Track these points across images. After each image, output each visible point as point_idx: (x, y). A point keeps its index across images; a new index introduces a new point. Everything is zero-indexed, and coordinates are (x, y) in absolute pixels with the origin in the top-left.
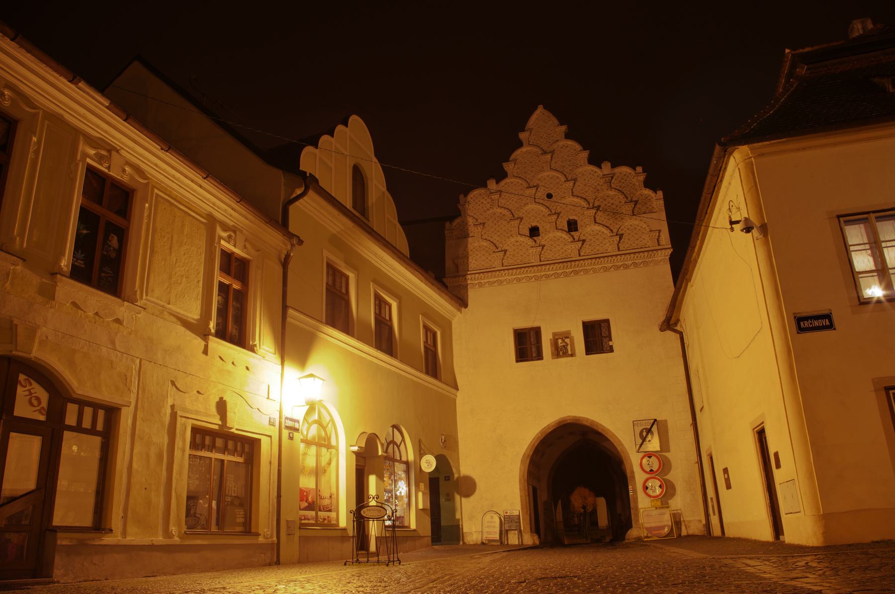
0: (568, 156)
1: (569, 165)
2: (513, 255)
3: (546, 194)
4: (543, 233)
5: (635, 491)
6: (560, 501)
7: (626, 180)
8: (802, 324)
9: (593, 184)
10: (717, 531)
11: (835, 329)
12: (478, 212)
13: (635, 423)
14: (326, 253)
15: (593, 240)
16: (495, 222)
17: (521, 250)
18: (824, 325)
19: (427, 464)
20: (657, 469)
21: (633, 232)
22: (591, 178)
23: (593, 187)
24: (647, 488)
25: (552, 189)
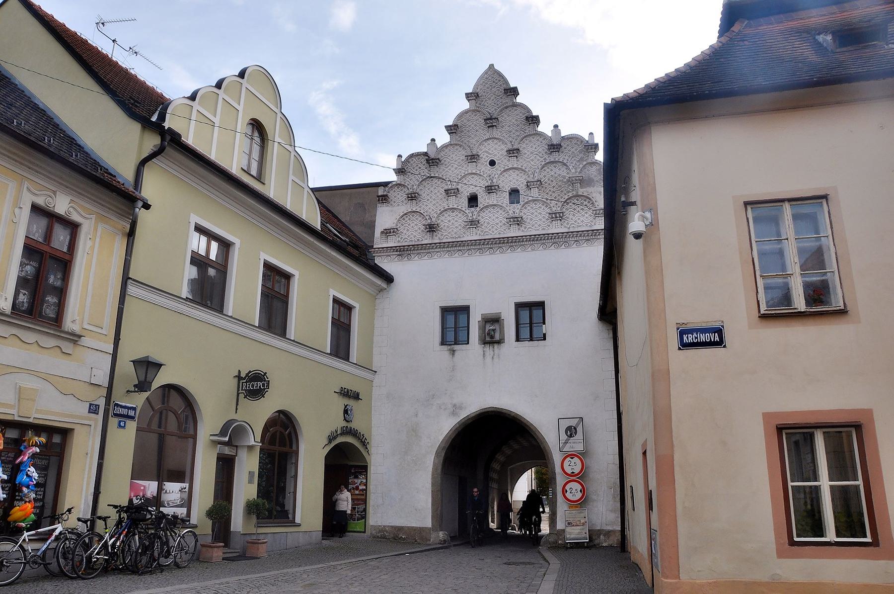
0: (516, 120)
2: (448, 227)
3: (489, 161)
8: (685, 338)
9: (540, 152)
11: (725, 346)
15: (535, 213)
17: (456, 221)
18: (713, 340)
21: (578, 207)
22: (539, 146)
23: (541, 155)
25: (495, 155)
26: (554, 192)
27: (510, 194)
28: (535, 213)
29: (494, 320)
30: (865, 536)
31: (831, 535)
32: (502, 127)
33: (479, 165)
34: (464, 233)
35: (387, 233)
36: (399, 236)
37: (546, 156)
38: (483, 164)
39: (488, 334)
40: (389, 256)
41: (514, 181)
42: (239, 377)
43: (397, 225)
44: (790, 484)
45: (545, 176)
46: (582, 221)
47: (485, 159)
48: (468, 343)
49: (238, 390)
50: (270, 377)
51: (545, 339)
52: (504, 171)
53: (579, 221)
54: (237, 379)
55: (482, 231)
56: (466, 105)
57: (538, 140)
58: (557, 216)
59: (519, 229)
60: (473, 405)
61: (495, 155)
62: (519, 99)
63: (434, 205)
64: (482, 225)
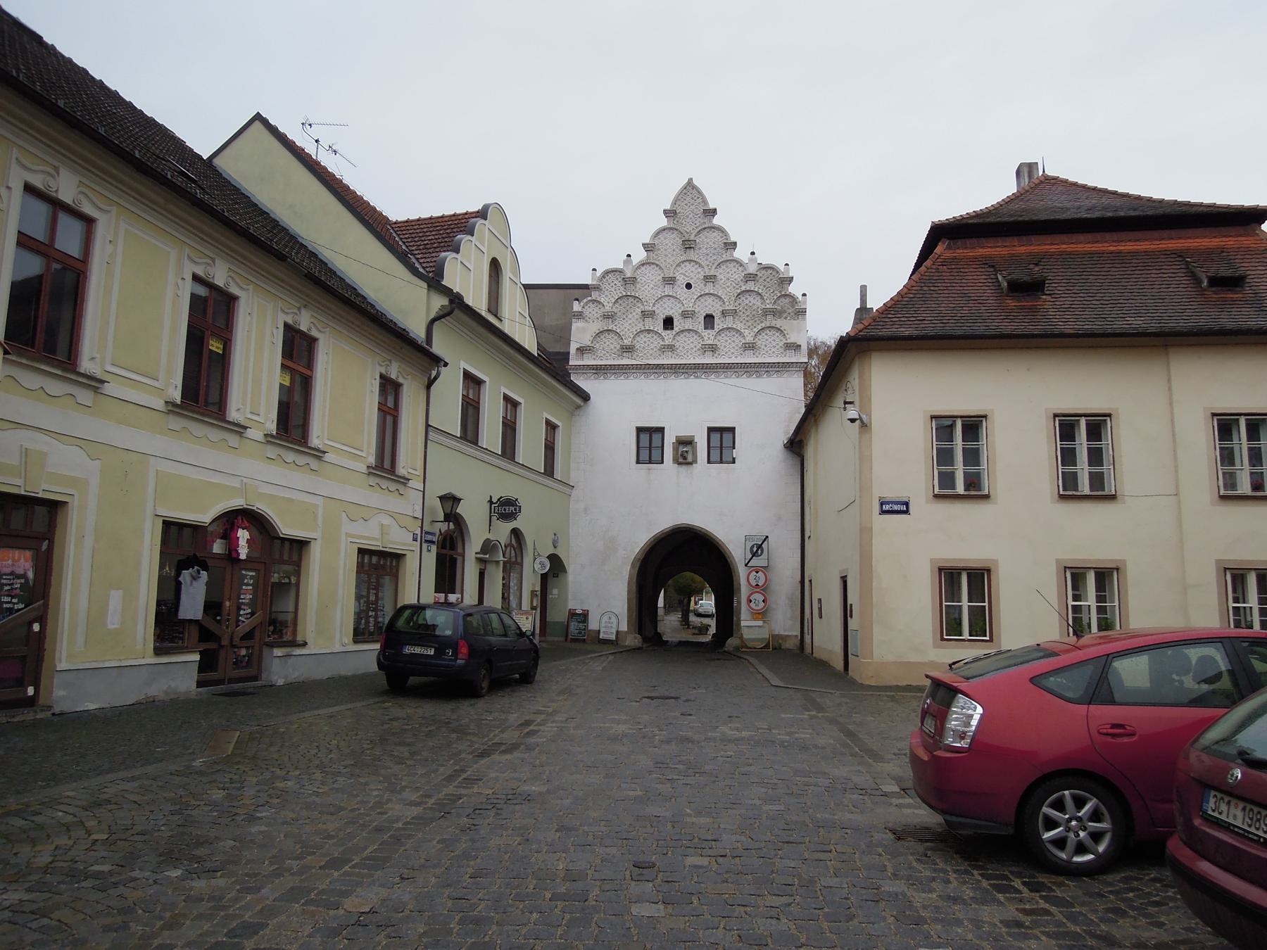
0: (714, 243)
1: (714, 254)
2: (644, 348)
4: (677, 326)
5: (739, 603)
6: (663, 591)
7: (771, 280)
10: (808, 650)
12: (610, 294)
13: (747, 538)
14: (462, 363)
15: (729, 341)
16: (628, 308)
17: (652, 343)
19: (540, 566)
20: (763, 583)
24: (751, 601)
26: (747, 321)
27: (705, 318)
28: (729, 341)
29: (685, 443)
30: (986, 636)
31: (966, 635)
32: (700, 249)
33: (676, 287)
34: (660, 355)
35: (582, 351)
36: (594, 354)
37: (742, 284)
38: (679, 286)
39: (682, 455)
40: (586, 373)
41: (710, 307)
42: (491, 502)
43: (592, 342)
44: (944, 603)
45: (740, 304)
46: (774, 352)
47: (682, 281)
48: (662, 463)
49: (491, 513)
50: (521, 502)
51: (734, 462)
52: (701, 296)
53: (770, 352)
54: (489, 504)
55: (677, 355)
56: (663, 222)
57: (734, 266)
58: (750, 347)
59: (713, 356)
60: (664, 522)
61: (691, 278)
62: (717, 221)
63: (630, 324)
64: (677, 349)
